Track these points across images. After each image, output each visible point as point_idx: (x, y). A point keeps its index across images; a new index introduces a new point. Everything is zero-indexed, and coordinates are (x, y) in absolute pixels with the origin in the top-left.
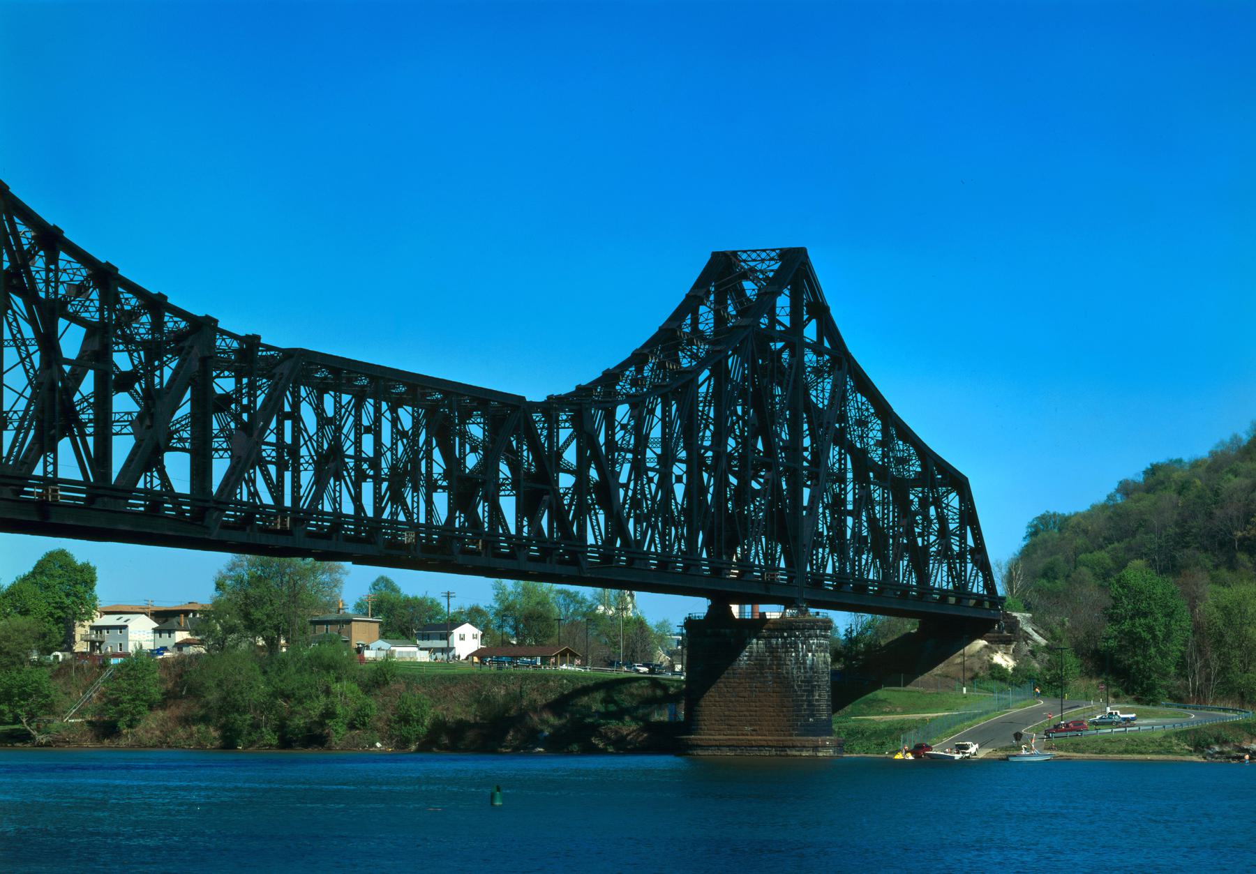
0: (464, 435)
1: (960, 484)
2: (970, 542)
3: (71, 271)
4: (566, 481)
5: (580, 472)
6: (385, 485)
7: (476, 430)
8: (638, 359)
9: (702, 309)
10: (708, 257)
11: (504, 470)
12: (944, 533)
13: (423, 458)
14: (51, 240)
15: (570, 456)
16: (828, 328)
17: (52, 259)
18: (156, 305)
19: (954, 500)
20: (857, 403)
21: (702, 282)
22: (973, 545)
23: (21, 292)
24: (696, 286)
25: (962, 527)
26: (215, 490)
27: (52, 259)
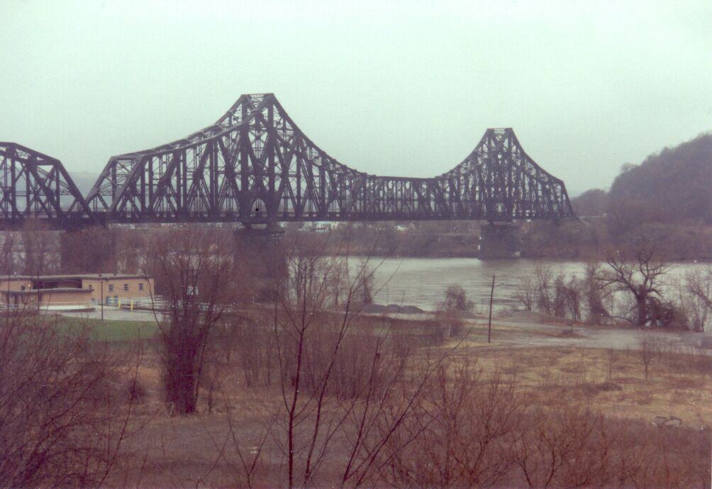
0: (422, 187)
1: (561, 183)
2: (564, 198)
3: (315, 153)
4: (447, 196)
5: (451, 193)
6: (181, 159)
7: (425, 186)
8: (466, 161)
9: (484, 145)
10: (486, 130)
11: (432, 196)
12: (556, 197)
13: (413, 192)
14: (311, 144)
15: (448, 190)
16: (519, 146)
17: (311, 149)
18: (334, 162)
19: (559, 187)
20: (528, 165)
21: (484, 138)
22: (237, 180)
23: (336, 302)
24: (483, 138)
25: (562, 195)
26: (268, 159)
27: (311, 149)
